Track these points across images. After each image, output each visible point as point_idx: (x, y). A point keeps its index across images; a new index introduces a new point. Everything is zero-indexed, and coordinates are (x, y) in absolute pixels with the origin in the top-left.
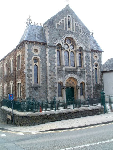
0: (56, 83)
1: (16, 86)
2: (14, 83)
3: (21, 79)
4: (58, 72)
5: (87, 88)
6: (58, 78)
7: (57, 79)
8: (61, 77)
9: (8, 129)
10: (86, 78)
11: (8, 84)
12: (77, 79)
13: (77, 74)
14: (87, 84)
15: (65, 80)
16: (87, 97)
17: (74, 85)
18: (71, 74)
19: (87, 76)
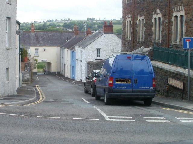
1: (170, 22)
2: (164, 16)
3: (184, 6)
9: (187, 107)
11: (149, 17)
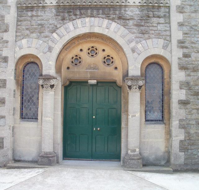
0: (5, 59)
4: (19, 16)
5: (185, 85)
6: (18, 38)
7: (10, 44)
8: (34, 35)
10: (177, 35)
12: (121, 41)
13: (120, 18)
14: (182, 68)
15: (50, 49)
16: (178, 136)
17: (116, 71)
18: (87, 20)
19: (185, 29)
